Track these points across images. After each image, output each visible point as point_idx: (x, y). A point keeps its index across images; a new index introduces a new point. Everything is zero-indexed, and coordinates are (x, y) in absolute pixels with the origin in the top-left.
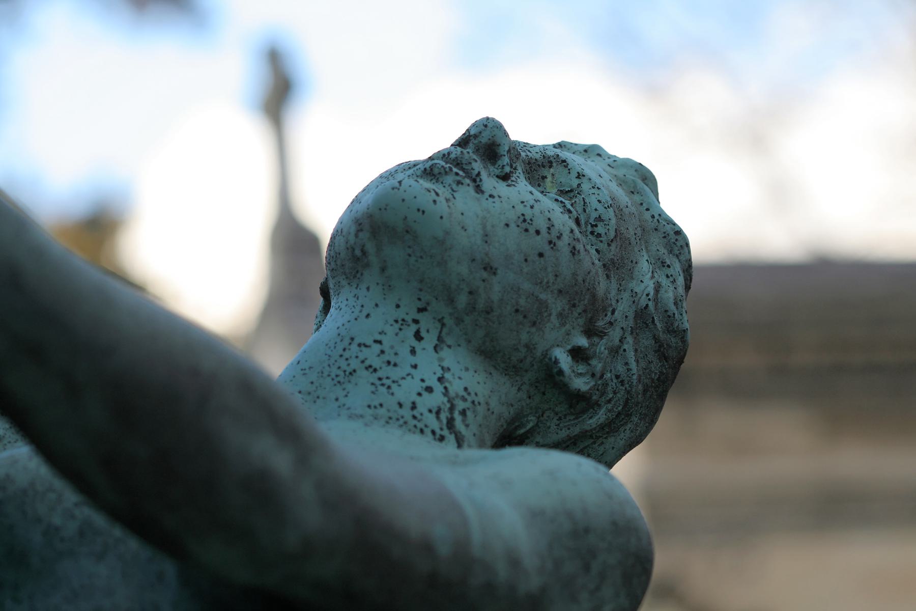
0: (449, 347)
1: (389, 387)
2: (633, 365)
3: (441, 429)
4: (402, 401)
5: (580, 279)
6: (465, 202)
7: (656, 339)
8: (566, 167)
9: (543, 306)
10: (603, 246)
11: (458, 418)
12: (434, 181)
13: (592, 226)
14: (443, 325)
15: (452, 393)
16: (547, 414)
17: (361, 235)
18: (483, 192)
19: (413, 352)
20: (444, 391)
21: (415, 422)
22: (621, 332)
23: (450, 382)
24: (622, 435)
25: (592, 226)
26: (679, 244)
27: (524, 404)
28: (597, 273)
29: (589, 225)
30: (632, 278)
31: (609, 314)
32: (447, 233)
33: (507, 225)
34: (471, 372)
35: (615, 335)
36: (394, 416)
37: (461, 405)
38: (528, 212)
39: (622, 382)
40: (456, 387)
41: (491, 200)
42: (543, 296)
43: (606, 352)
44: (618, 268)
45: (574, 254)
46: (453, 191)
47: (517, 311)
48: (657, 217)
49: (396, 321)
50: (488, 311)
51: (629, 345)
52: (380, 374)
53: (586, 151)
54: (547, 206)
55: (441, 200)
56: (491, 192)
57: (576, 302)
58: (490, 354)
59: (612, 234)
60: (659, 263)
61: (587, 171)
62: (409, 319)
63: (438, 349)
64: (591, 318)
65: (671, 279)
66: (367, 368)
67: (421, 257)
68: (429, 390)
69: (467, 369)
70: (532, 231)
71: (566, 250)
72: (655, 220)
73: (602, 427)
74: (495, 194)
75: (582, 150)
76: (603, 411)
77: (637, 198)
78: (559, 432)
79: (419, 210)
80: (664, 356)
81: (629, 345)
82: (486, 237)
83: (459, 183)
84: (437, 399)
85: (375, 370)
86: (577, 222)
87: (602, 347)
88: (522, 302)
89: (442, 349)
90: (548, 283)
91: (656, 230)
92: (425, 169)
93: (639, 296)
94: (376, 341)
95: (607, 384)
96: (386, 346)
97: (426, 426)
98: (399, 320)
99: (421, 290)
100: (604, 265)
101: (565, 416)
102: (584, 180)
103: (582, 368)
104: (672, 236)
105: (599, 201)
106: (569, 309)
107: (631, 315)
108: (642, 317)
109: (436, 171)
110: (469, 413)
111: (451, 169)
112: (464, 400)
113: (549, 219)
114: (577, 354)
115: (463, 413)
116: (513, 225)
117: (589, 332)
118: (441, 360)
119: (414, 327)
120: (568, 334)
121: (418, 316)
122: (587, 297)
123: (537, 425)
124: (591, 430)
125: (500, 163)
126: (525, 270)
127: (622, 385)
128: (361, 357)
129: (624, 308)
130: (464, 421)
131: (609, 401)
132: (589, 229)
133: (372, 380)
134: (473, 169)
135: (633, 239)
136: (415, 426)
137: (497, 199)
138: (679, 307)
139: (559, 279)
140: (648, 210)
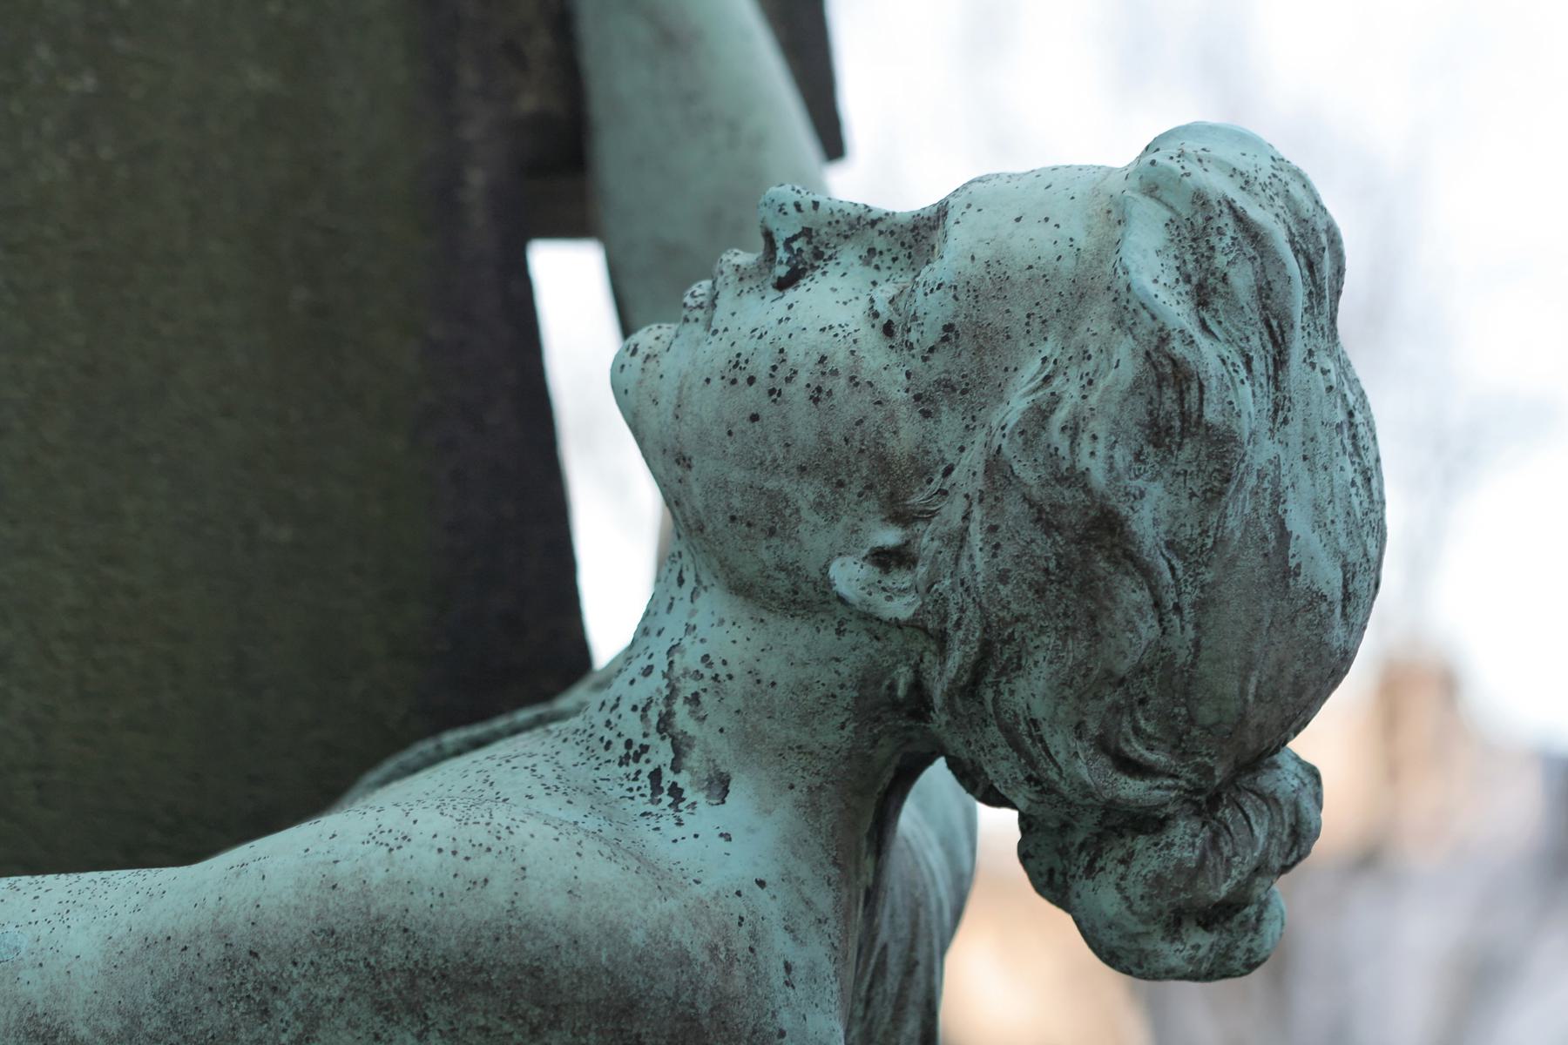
5: (836, 438)
9: (777, 503)
22: (965, 503)
24: (1035, 672)
26: (1131, 307)
27: (872, 651)
28: (891, 417)
31: (938, 477)
34: (727, 625)
35: (952, 511)
37: (689, 687)
40: (690, 658)
42: (771, 484)
45: (816, 400)
47: (733, 518)
57: (843, 477)
64: (892, 495)
87: (927, 541)
88: (736, 502)
90: (774, 460)
95: (945, 600)
106: (832, 493)
110: (704, 698)
112: (698, 676)
113: (782, 351)
115: (695, 699)
116: (716, 381)
117: (901, 517)
126: (731, 450)
130: (692, 713)
131: (958, 625)
135: (1018, 330)
139: (793, 450)
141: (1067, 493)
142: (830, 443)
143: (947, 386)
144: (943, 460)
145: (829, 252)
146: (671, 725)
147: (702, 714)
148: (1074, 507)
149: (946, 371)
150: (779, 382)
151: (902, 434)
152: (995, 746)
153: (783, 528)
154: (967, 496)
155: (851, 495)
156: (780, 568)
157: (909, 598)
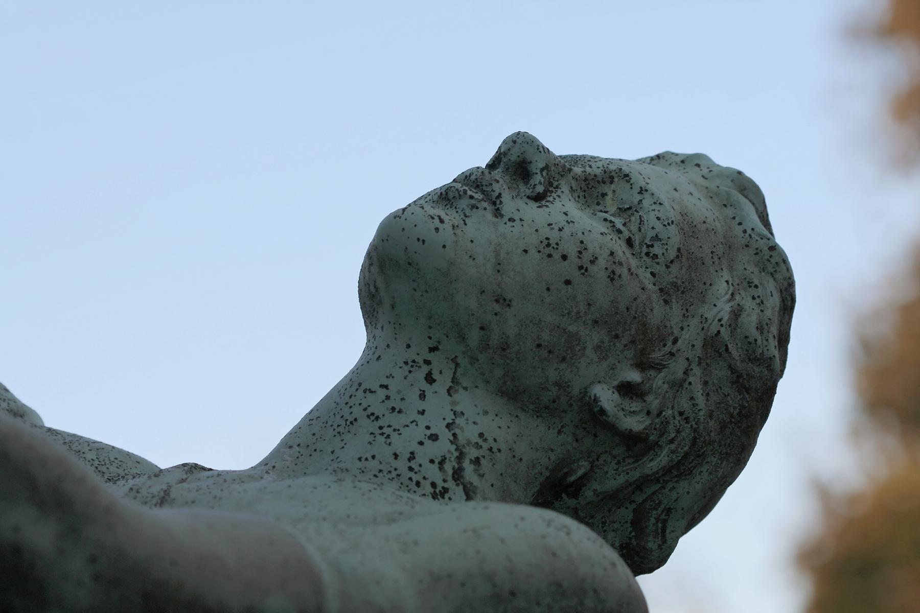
0: (466, 389)
1: (388, 437)
2: (701, 400)
3: (445, 481)
4: (398, 453)
5: (622, 307)
6: (480, 228)
7: (732, 369)
8: (628, 181)
10: (660, 269)
11: (468, 468)
12: (448, 206)
13: (648, 246)
14: (457, 365)
15: (462, 440)
16: (604, 457)
17: (372, 269)
18: (502, 216)
19: (422, 396)
20: (452, 438)
21: (411, 474)
22: (687, 363)
23: (462, 428)
24: (698, 478)
25: (648, 246)
26: (773, 261)
27: (571, 449)
28: (649, 299)
29: (642, 246)
30: (704, 302)
31: (669, 344)
32: (452, 264)
33: (526, 251)
34: (491, 416)
35: (677, 367)
36: (385, 468)
37: (473, 453)
38: (554, 235)
39: (687, 419)
40: (468, 433)
41: (511, 224)
42: (572, 328)
43: (666, 386)
44: (683, 290)
45: (612, 279)
46: (466, 216)
48: (749, 231)
49: (406, 363)
50: (504, 347)
51: (696, 377)
52: (381, 422)
53: (683, 162)
54: (587, 224)
55: (447, 226)
56: (511, 216)
58: (513, 394)
59: (672, 254)
60: (745, 284)
61: (652, 187)
62: (420, 360)
63: (452, 392)
64: (643, 349)
65: (758, 301)
66: (368, 416)
67: (427, 292)
68: (434, 437)
69: (486, 413)
70: (557, 256)
71: (602, 276)
72: (747, 235)
73: (667, 470)
74: (517, 218)
75: (679, 160)
76: (665, 452)
77: (729, 212)
78: (617, 477)
79: (418, 239)
80: (744, 387)
81: (696, 377)
82: (499, 268)
83: (474, 207)
84: (444, 446)
85: (377, 418)
86: (629, 242)
87: (659, 381)
88: (545, 335)
89: (457, 391)
90: (578, 313)
91: (747, 246)
92: (441, 193)
93: (709, 322)
94: (381, 386)
96: (392, 392)
97: (424, 478)
98: (409, 361)
99: (430, 327)
100: (661, 290)
101: (624, 459)
102: (646, 195)
103: (636, 406)
104: (766, 253)
105: (658, 219)
107: (699, 344)
108: (713, 346)
109: (451, 195)
110: (483, 461)
111: (465, 192)
112: (478, 446)
113: (582, 242)
114: (627, 390)
115: (477, 461)
117: (642, 365)
118: (454, 403)
119: (425, 369)
120: (613, 369)
121: (430, 357)
122: (634, 326)
123: (592, 469)
124: (653, 474)
125: (532, 182)
127: (687, 423)
128: (365, 405)
129: (690, 337)
130: (475, 471)
131: (672, 441)
132: (645, 250)
133: (371, 430)
134: (493, 191)
135: (708, 260)
136: (410, 479)
137: (518, 222)
138: (765, 331)
139: (592, 309)
140: (740, 224)
141: (756, 369)
142: (618, 308)
143: (675, 286)
144: (673, 333)
145: (555, 184)
146: (463, 477)
147: (481, 472)
148: (761, 378)
149: (676, 277)
150: (585, 261)
151: (655, 311)
152: (614, 522)
153: (571, 358)
154: (688, 359)
155: (619, 346)
156: (557, 384)
157: (639, 418)
